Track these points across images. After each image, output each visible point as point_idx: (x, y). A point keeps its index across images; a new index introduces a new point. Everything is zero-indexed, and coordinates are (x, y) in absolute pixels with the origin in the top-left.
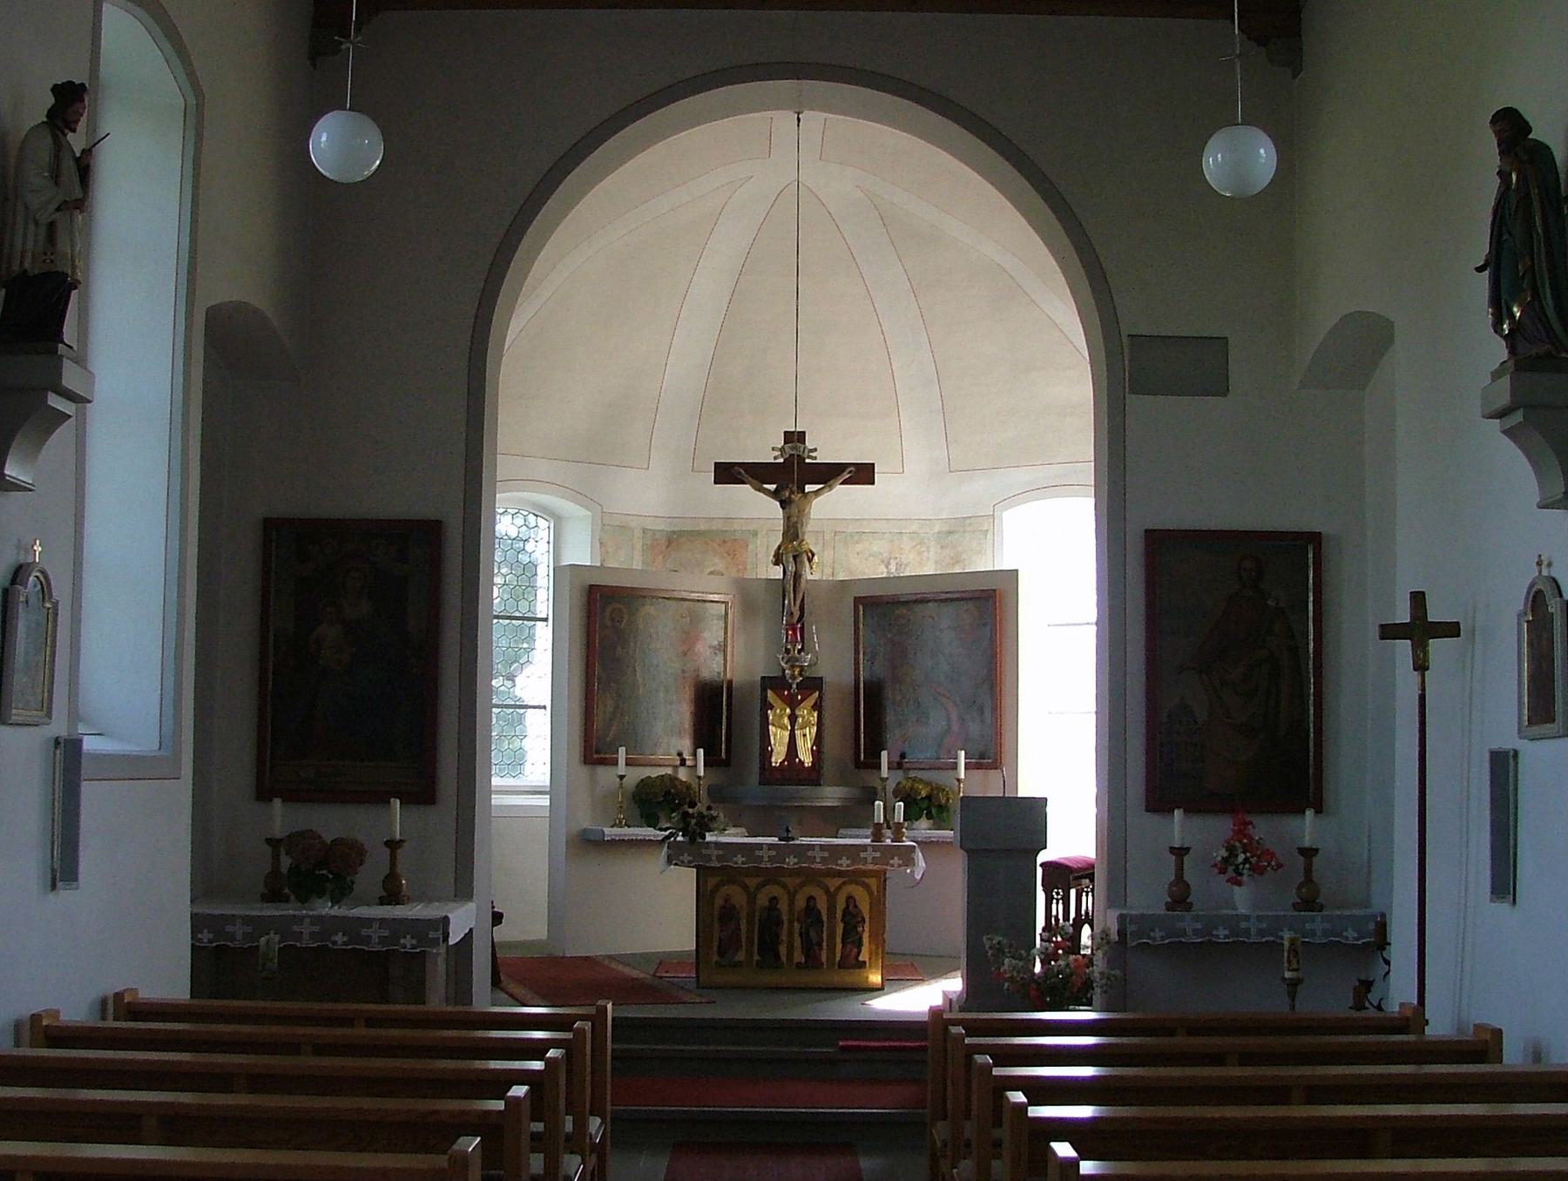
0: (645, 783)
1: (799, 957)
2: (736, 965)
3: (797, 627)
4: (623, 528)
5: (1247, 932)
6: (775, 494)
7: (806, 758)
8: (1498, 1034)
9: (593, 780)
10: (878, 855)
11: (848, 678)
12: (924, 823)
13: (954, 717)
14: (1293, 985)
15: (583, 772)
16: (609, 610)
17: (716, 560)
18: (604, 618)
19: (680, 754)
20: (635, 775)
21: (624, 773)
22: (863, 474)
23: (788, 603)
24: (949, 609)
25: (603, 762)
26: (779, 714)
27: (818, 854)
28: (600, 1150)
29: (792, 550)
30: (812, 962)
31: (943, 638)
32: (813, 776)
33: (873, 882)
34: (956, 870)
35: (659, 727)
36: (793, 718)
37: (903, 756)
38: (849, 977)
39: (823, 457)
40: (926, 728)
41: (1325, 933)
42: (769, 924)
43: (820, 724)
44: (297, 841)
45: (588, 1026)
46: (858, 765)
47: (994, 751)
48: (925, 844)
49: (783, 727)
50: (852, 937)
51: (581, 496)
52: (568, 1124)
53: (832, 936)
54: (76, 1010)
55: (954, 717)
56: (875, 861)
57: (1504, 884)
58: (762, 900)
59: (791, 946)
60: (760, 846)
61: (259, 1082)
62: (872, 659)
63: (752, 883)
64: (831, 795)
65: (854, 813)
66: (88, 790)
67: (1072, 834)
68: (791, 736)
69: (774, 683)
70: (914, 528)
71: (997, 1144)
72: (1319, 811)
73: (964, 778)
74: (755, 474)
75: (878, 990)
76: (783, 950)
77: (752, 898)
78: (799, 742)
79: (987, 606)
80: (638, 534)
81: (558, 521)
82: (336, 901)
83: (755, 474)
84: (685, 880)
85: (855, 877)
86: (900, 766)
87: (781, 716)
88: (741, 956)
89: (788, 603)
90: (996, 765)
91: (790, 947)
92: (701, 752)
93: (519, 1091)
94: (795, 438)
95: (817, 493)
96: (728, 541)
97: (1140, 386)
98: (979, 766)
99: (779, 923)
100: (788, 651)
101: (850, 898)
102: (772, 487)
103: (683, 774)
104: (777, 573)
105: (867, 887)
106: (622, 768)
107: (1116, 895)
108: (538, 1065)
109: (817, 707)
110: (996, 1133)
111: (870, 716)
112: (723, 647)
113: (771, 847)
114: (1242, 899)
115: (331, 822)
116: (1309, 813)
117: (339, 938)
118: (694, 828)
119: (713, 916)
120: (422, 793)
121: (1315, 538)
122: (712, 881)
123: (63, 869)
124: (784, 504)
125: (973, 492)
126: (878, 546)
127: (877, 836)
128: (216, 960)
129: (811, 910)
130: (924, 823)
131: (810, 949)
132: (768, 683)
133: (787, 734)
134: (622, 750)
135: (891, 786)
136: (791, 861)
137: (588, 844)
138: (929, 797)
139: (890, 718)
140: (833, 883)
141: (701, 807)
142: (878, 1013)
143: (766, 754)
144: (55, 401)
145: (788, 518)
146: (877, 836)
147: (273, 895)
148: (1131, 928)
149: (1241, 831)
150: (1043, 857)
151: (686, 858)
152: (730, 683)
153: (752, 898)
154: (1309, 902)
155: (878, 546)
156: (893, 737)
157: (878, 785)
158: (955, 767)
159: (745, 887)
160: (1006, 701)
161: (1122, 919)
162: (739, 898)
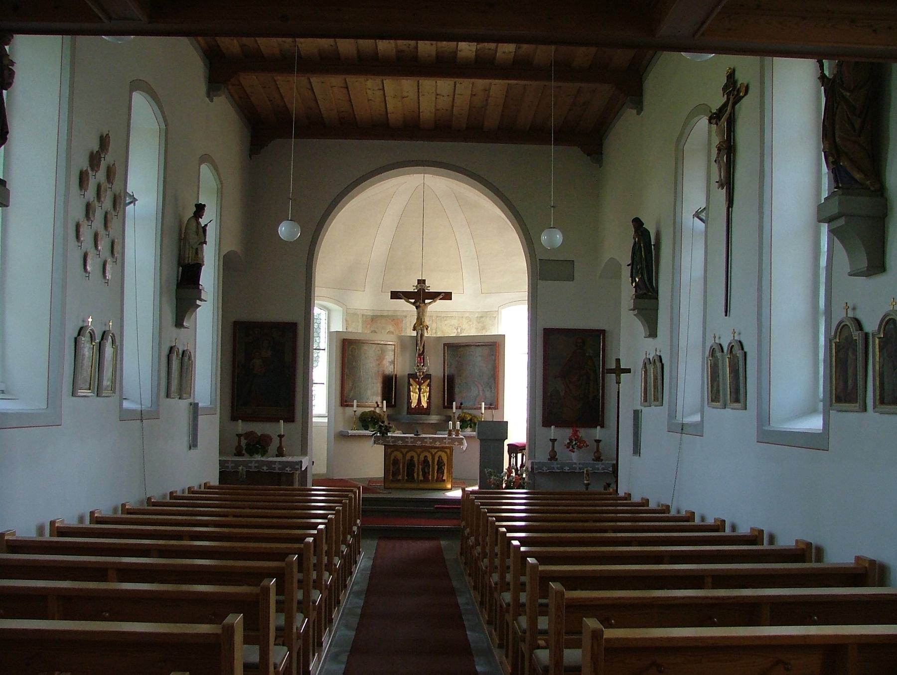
0: (364, 414)
1: (421, 478)
2: (399, 480)
3: (422, 355)
4: (354, 314)
5: (575, 469)
6: (414, 304)
7: (425, 405)
8: (648, 500)
9: (344, 413)
12: (469, 429)
13: (481, 389)
14: (588, 484)
15: (340, 409)
17: (391, 327)
18: (348, 350)
20: (360, 410)
21: (356, 410)
22: (448, 296)
23: (419, 346)
24: (479, 349)
25: (347, 406)
26: (414, 388)
28: (329, 588)
29: (420, 325)
30: (426, 480)
31: (478, 359)
32: (427, 412)
33: (448, 451)
34: (477, 445)
35: (369, 392)
36: (420, 390)
38: (439, 486)
40: (470, 392)
41: (603, 469)
42: (411, 465)
43: (430, 392)
44: (249, 435)
45: (333, 517)
46: (444, 407)
47: (495, 404)
48: (468, 438)
50: (440, 470)
51: (339, 302)
52: (314, 575)
53: (433, 470)
54: (69, 519)
55: (481, 389)
56: (449, 443)
57: (637, 450)
58: (408, 457)
59: (418, 474)
60: (407, 438)
61: (163, 552)
62: (450, 366)
63: (404, 451)
64: (434, 419)
65: (441, 426)
66: (200, 417)
67: (517, 434)
68: (419, 396)
69: (412, 376)
70: (468, 315)
71: (523, 584)
72: (602, 427)
73: (484, 414)
74: (406, 295)
75: (451, 490)
76: (415, 475)
77: (404, 456)
78: (422, 398)
79: (493, 348)
80: (360, 316)
81: (329, 311)
82: (262, 456)
83: (406, 295)
84: (381, 449)
85: (442, 449)
86: (460, 408)
88: (400, 477)
89: (419, 346)
90: (496, 408)
91: (418, 475)
93: (311, 539)
94: (421, 282)
95: (430, 303)
96: (395, 320)
97: (543, 278)
98: (489, 408)
99: (414, 466)
101: (440, 457)
102: (413, 301)
103: (378, 410)
104: (414, 334)
105: (446, 453)
106: (355, 408)
107: (532, 455)
108: (315, 532)
109: (429, 385)
110: (523, 579)
111: (450, 388)
112: (393, 362)
114: (575, 457)
115: (259, 428)
116: (598, 428)
117: (265, 468)
118: (384, 431)
119: (391, 464)
120: (290, 418)
121: (603, 332)
122: (389, 451)
123: (193, 444)
124: (417, 308)
125: (490, 302)
126: (454, 322)
127: (450, 434)
128: (224, 475)
129: (426, 461)
130: (469, 429)
131: (425, 474)
135: (456, 416)
136: (419, 443)
137: (343, 436)
138: (471, 420)
139: (457, 390)
140: (434, 451)
141: (386, 423)
143: (409, 403)
144: (198, 302)
145: (418, 313)
146: (450, 434)
147: (239, 453)
148: (535, 467)
149: (575, 433)
150: (506, 442)
151: (381, 441)
153: (404, 456)
154: (598, 459)
155: (454, 322)
156: (457, 397)
157: (452, 415)
158: (481, 408)
159: (401, 452)
160: (500, 386)
161: (532, 463)
162: (400, 456)
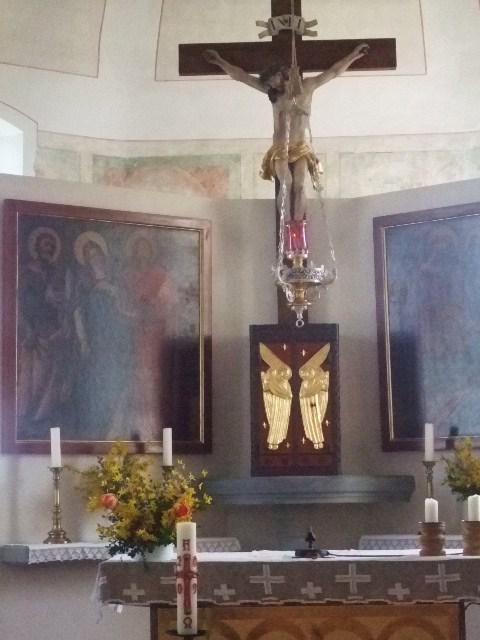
7: (315, 434)
10: (457, 577)
11: (370, 332)
16: (33, 238)
19: (136, 437)
22: (379, 54)
26: (276, 375)
27: (353, 579)
32: (326, 461)
36: (296, 383)
37: (454, 431)
39: (325, 32)
46: (388, 447)
49: (281, 395)
60: (256, 567)
87: (280, 381)
92: (168, 433)
100: (288, 262)
104: (266, 190)
109: (330, 365)
113: (276, 567)
124: (274, 95)
127: (432, 543)
132: (259, 334)
133: (287, 404)
134: (55, 433)
142: (18, 125)
146: (432, 543)
151: (134, 591)
152: (208, 342)
156: (433, 404)
